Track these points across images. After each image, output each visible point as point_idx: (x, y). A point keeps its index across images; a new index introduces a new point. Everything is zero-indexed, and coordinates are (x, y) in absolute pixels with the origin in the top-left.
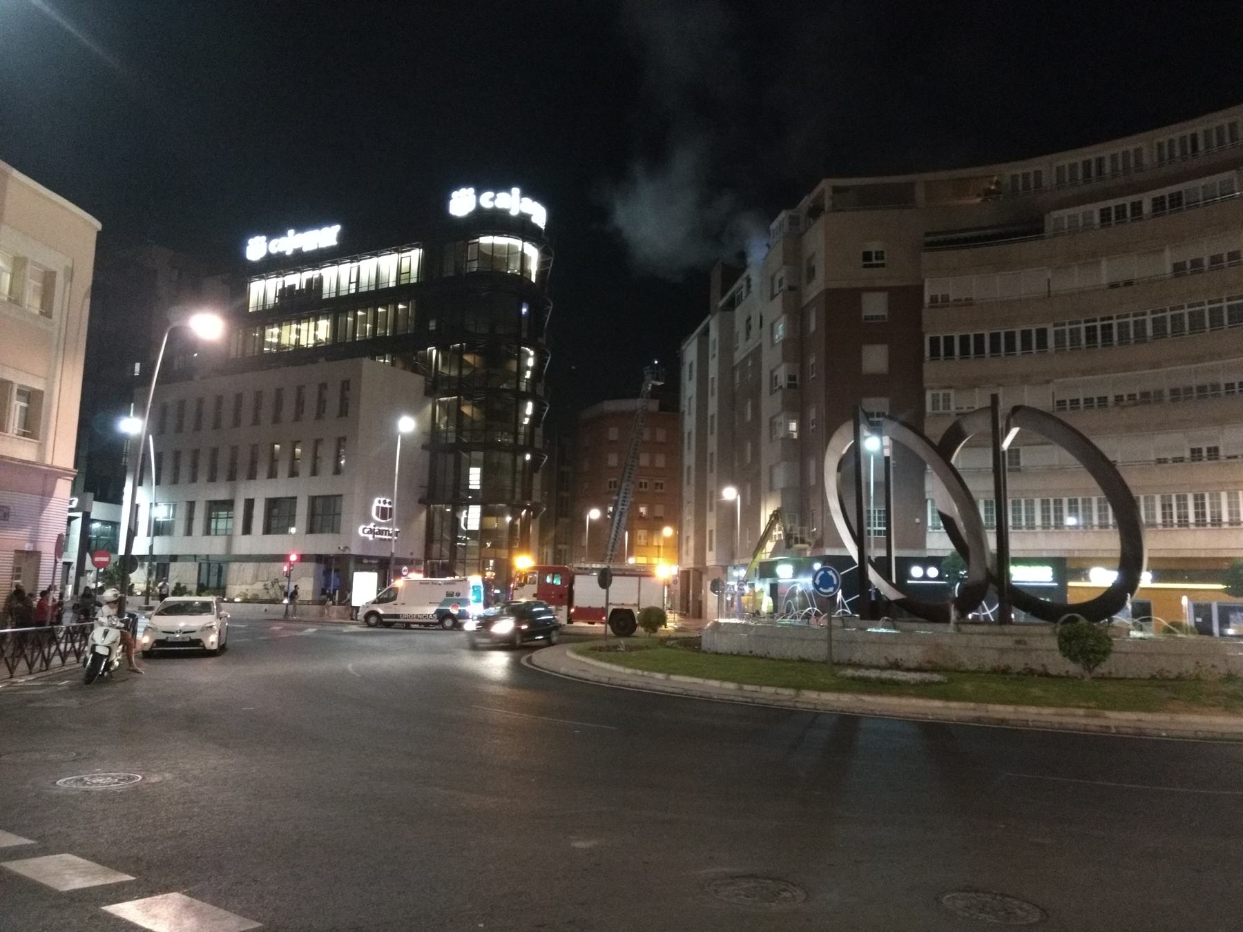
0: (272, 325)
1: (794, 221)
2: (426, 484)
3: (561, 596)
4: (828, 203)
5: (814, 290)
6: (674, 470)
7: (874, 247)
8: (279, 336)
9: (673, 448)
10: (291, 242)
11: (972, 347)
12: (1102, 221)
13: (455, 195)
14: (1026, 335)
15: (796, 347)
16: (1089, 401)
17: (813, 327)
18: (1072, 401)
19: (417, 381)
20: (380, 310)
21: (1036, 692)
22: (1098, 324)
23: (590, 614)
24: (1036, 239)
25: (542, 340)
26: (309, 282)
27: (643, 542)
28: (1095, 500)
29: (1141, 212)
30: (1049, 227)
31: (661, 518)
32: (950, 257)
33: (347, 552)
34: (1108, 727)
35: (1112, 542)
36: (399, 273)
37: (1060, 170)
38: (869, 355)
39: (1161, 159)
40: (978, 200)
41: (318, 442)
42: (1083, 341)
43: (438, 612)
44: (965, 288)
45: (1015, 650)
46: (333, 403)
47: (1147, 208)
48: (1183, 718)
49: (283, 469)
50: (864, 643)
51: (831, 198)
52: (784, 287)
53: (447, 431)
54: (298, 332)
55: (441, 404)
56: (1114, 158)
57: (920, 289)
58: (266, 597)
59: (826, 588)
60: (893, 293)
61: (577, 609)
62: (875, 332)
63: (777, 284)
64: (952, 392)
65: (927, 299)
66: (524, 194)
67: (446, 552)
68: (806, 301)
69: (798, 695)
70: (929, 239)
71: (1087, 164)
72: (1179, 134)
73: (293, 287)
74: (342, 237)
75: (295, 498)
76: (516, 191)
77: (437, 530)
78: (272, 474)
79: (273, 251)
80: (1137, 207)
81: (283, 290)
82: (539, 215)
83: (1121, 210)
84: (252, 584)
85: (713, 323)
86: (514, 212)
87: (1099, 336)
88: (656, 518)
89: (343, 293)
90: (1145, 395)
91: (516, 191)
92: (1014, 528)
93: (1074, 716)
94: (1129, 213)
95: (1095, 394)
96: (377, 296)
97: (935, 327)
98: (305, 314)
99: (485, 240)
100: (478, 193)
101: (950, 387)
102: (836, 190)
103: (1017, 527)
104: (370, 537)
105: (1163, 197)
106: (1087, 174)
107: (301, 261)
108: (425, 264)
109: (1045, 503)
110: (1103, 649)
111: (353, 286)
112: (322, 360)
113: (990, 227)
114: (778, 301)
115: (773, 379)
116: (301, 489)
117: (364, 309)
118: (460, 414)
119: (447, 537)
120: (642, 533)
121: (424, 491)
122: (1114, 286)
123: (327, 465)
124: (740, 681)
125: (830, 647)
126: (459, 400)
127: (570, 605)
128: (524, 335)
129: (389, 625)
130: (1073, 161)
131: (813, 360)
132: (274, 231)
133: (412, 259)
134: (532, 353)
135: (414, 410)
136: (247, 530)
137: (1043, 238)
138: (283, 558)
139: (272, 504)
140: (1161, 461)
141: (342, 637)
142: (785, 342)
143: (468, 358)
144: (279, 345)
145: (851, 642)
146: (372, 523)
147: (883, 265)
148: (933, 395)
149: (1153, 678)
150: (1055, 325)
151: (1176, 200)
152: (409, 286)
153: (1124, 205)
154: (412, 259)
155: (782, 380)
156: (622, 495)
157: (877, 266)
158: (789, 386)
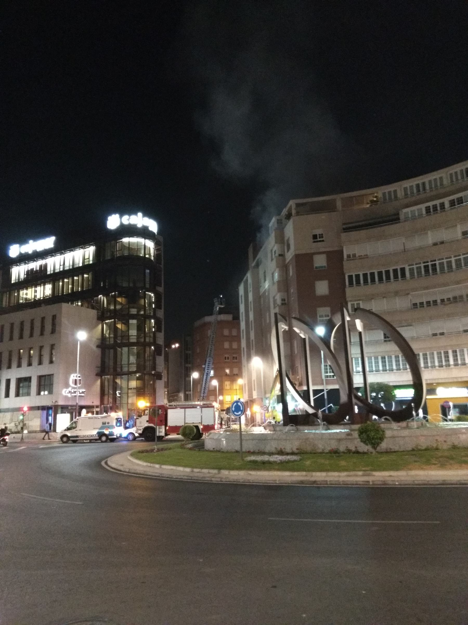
0: (23, 289)
1: (279, 222)
2: (99, 365)
3: (161, 421)
4: (294, 212)
5: (289, 256)
6: (238, 350)
7: (318, 232)
8: (26, 294)
9: (238, 338)
10: (32, 246)
11: (369, 279)
12: (427, 213)
13: (109, 218)
14: (395, 271)
15: (284, 285)
16: (428, 303)
17: (291, 274)
18: (420, 303)
19: (93, 313)
20: (75, 278)
21: (343, 463)
23: (175, 429)
24: (396, 223)
25: (161, 289)
26: (41, 266)
27: (228, 387)
28: (400, 356)
29: (444, 208)
30: (402, 217)
31: (237, 374)
32: (354, 234)
33: (57, 404)
34: (368, 482)
35: (407, 377)
36: (84, 259)
37: (405, 189)
39: (452, 181)
40: (368, 206)
41: (41, 348)
43: (98, 433)
44: (365, 250)
45: (346, 439)
46: (48, 327)
47: (447, 205)
48: (413, 473)
49: (24, 362)
50: (270, 440)
51: (295, 209)
52: (277, 255)
53: (110, 338)
54: (36, 291)
55: (106, 323)
56: (430, 182)
57: (342, 252)
58: (16, 430)
59: (238, 412)
60: (329, 255)
61: (169, 427)
62: (321, 274)
63: (273, 253)
64: (361, 302)
65: (345, 257)
66: (145, 215)
67: (111, 400)
68: (287, 261)
69: (219, 473)
70: (344, 226)
71: (418, 186)
72: (460, 169)
73: (32, 270)
74: (56, 243)
75: (53, 375)
76: (140, 214)
77: (106, 389)
79: (23, 252)
80: (442, 205)
81: (28, 272)
82: (153, 226)
83: (435, 207)
84: (10, 423)
85: (249, 275)
86: (139, 226)
87: (430, 269)
88: (234, 375)
89: (57, 271)
90: (455, 298)
91: (140, 214)
92: (425, 368)
93: (357, 476)
95: (431, 299)
96: (74, 271)
97: (350, 270)
98: (39, 282)
99: (126, 240)
100: (121, 216)
101: (360, 300)
102: (298, 205)
103: (371, 371)
104: (69, 395)
105: (454, 200)
106: (418, 190)
107: (37, 256)
108: (97, 254)
110: (379, 436)
112: (43, 305)
113: (364, 221)
114: (274, 261)
115: (275, 301)
116: (33, 372)
117: (68, 278)
118: (116, 329)
119: (111, 392)
121: (99, 369)
122: (435, 244)
123: (46, 359)
124: (192, 467)
125: (241, 444)
126: (115, 322)
127: (166, 425)
128: (148, 286)
129: (75, 442)
130: (411, 184)
131: (292, 291)
132: (22, 241)
133: (89, 252)
134: (152, 295)
135: (90, 328)
136: (7, 395)
137: (399, 222)
138: (20, 409)
139: (19, 381)
140: (435, 335)
141: (53, 450)
142: (279, 282)
143: (119, 300)
144: (26, 299)
145: (265, 440)
146: (72, 386)
147: (323, 241)
148: (352, 304)
149: (413, 450)
150: (409, 265)
151: (460, 201)
152: (89, 265)
154: (89, 252)
155: (279, 302)
156: (207, 364)
157: (320, 241)
158: (282, 304)
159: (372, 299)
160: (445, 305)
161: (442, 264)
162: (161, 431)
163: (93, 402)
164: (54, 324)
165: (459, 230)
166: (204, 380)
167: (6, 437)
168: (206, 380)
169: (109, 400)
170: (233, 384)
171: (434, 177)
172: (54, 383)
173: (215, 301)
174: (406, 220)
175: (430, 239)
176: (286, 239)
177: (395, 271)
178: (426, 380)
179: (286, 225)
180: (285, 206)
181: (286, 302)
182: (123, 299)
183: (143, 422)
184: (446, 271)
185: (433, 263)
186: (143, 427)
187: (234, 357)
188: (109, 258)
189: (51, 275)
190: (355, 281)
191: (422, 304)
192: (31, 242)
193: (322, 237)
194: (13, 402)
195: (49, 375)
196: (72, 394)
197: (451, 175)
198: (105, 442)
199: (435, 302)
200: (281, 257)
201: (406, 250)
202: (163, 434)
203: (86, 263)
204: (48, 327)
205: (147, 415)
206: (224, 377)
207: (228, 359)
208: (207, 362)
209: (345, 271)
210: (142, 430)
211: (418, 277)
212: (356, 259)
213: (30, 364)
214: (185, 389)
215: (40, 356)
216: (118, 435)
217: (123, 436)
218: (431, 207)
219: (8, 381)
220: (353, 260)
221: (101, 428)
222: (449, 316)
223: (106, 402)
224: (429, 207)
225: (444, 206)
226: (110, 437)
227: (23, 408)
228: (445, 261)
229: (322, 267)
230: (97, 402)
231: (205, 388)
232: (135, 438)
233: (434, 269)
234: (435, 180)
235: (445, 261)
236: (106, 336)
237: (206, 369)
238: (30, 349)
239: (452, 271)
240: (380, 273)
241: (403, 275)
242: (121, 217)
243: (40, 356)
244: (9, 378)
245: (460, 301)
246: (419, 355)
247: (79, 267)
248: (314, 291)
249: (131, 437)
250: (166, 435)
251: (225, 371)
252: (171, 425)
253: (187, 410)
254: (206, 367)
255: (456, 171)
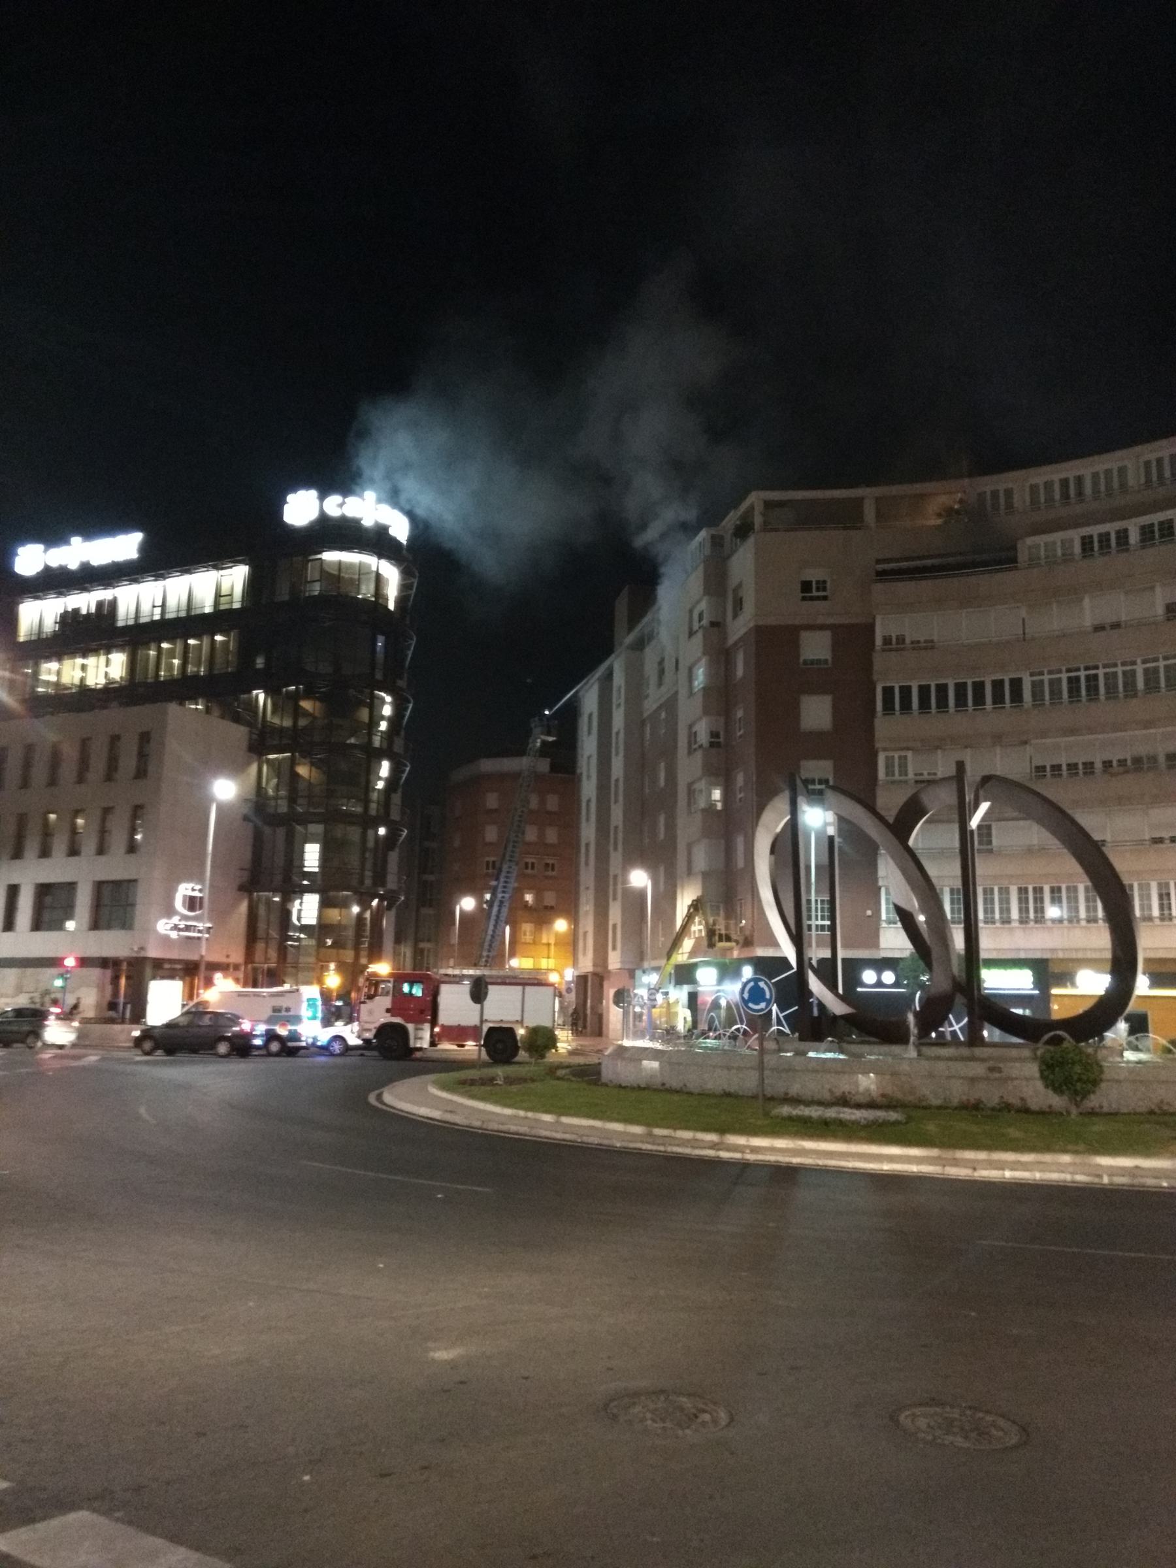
0: (48, 658)
4: (758, 520)
5: (739, 627)
10: (77, 552)
11: (932, 699)
12: (1084, 550)
13: (291, 498)
14: (998, 685)
15: (721, 696)
16: (1072, 767)
17: (740, 672)
19: (239, 733)
22: (1082, 674)
23: (459, 1034)
24: (1010, 569)
26: (100, 605)
27: (528, 938)
28: (1081, 888)
29: (1127, 543)
30: (1023, 556)
31: (552, 908)
32: (905, 589)
33: (142, 954)
35: (1100, 939)
36: (218, 595)
37: (1034, 489)
38: (808, 711)
39: (1148, 480)
41: (107, 811)
42: (1065, 695)
45: (987, 1079)
46: (128, 763)
47: (1134, 537)
49: (60, 845)
52: (705, 622)
53: (276, 798)
54: (84, 668)
55: (268, 761)
56: (1095, 476)
57: (870, 628)
59: (757, 1003)
61: (443, 1026)
62: (815, 679)
64: (909, 754)
65: (879, 641)
67: (273, 954)
68: (731, 641)
70: (880, 567)
71: (1065, 483)
73: (76, 611)
74: (144, 548)
75: (135, 881)
77: (262, 926)
78: (45, 853)
79: (54, 564)
80: (1123, 536)
82: (400, 529)
83: (1104, 538)
86: (368, 522)
87: (1084, 688)
88: (546, 907)
90: (1137, 761)
92: (986, 922)
94: (1096, 545)
96: (188, 624)
97: (889, 673)
99: (330, 556)
101: (908, 749)
102: (769, 505)
103: (990, 921)
104: (174, 935)
106: (1065, 495)
107: (88, 577)
108: (253, 586)
109: (1023, 891)
111: (158, 611)
115: (692, 736)
116: (83, 873)
118: (295, 776)
120: (527, 928)
121: (246, 874)
122: (1099, 628)
123: (118, 840)
127: (434, 1023)
128: (379, 676)
131: (740, 714)
132: (53, 537)
135: (235, 769)
137: (1016, 568)
138: (55, 962)
139: (43, 890)
140: (1158, 841)
142: (706, 690)
143: (306, 705)
145: (787, 1071)
147: (825, 598)
148: (887, 758)
150: (1032, 675)
151: (1166, 529)
152: (231, 612)
153: (1108, 534)
155: (703, 738)
156: (502, 880)
157: (818, 598)
158: (712, 745)
159: (937, 748)
160: (1112, 775)
161: (1111, 678)
162: (421, 1037)
163: (228, 956)
164: (142, 756)
165: (1159, 600)
166: (493, 918)
167: (539, 1043)
168: (498, 917)
169: (270, 955)
170: (541, 929)
171: (1106, 467)
172: (138, 901)
173: (533, 725)
174: (1033, 562)
175: (1087, 612)
176: (733, 582)
177: (998, 685)
178: (1145, 949)
179: (733, 552)
180: (736, 506)
181: (721, 740)
182: (318, 704)
183: (377, 1013)
184: (1121, 695)
185: (1128, 668)
186: (377, 1025)
187: (547, 865)
188: (286, 598)
189: (127, 629)
190: (900, 701)
191: (1056, 768)
192: (76, 540)
193: (824, 589)
194: (24, 941)
195: (130, 881)
196: (182, 933)
197: (1147, 464)
198: (277, 1055)
199: (1089, 766)
200: (715, 629)
201: (1028, 636)
202: (425, 1044)
203: (222, 607)
204: (128, 763)
205: (387, 994)
206: (520, 912)
207: (533, 868)
208: (503, 874)
209: (875, 677)
210: (374, 1031)
211: (1126, 697)
212: (902, 649)
213: (73, 852)
214: (416, 934)
215: (103, 833)
216: (310, 1041)
217: (319, 1044)
218: (1096, 539)
219: (13, 892)
220: (897, 650)
221: (269, 1021)
222: (1123, 801)
223: (259, 955)
224: (1091, 537)
225: (1127, 537)
226: (290, 1044)
227: (63, 959)
228: (1120, 670)
229: (819, 661)
230: (237, 956)
231: (493, 936)
232: (348, 1049)
233: (1093, 688)
234: (1108, 472)
235: (1120, 670)
236: (266, 792)
237: (500, 890)
238: (77, 813)
239: (1135, 696)
240: (924, 691)
241: (1017, 696)
242: (322, 498)
243: (103, 833)
244: (16, 882)
245: (1149, 769)
246: (1131, 886)
247: (204, 616)
248: (797, 717)
249: (337, 1047)
250: (433, 1044)
251: (522, 897)
252: (446, 1023)
253: (528, 988)
254: (501, 884)
255: (1160, 454)
